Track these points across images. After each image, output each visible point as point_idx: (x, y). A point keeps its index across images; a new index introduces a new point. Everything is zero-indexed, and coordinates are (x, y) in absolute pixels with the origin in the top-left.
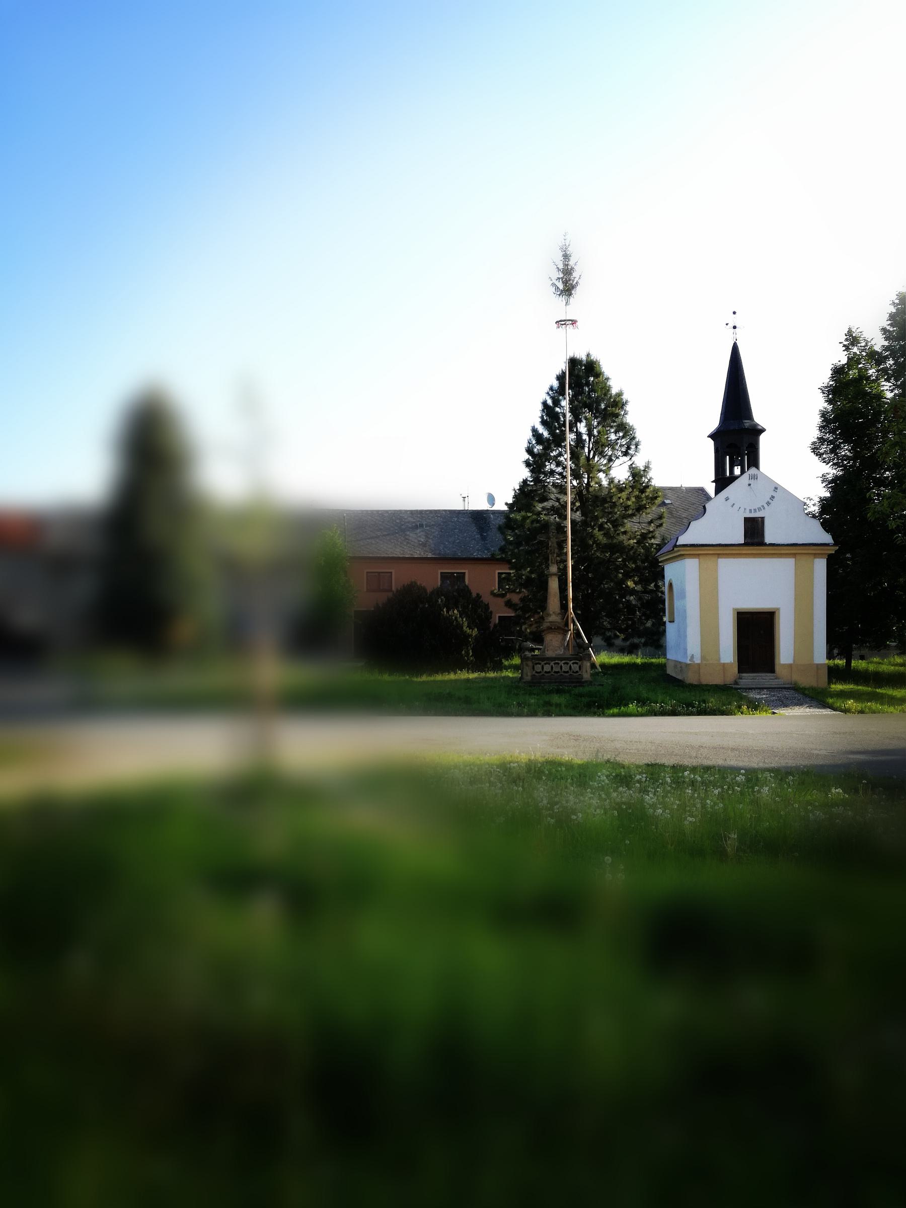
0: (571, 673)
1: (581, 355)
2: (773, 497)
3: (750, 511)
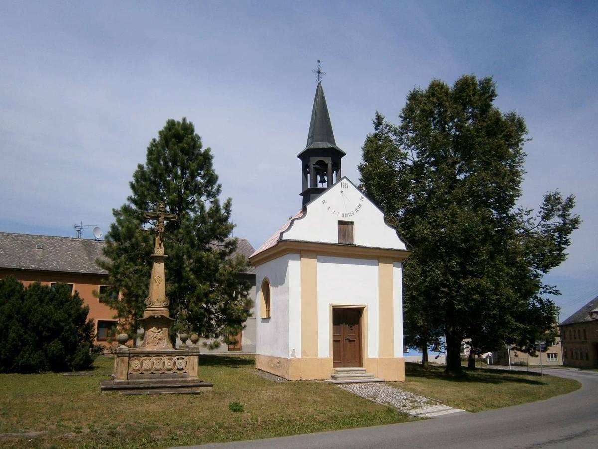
1: (178, 119)
2: (360, 205)
3: (343, 214)
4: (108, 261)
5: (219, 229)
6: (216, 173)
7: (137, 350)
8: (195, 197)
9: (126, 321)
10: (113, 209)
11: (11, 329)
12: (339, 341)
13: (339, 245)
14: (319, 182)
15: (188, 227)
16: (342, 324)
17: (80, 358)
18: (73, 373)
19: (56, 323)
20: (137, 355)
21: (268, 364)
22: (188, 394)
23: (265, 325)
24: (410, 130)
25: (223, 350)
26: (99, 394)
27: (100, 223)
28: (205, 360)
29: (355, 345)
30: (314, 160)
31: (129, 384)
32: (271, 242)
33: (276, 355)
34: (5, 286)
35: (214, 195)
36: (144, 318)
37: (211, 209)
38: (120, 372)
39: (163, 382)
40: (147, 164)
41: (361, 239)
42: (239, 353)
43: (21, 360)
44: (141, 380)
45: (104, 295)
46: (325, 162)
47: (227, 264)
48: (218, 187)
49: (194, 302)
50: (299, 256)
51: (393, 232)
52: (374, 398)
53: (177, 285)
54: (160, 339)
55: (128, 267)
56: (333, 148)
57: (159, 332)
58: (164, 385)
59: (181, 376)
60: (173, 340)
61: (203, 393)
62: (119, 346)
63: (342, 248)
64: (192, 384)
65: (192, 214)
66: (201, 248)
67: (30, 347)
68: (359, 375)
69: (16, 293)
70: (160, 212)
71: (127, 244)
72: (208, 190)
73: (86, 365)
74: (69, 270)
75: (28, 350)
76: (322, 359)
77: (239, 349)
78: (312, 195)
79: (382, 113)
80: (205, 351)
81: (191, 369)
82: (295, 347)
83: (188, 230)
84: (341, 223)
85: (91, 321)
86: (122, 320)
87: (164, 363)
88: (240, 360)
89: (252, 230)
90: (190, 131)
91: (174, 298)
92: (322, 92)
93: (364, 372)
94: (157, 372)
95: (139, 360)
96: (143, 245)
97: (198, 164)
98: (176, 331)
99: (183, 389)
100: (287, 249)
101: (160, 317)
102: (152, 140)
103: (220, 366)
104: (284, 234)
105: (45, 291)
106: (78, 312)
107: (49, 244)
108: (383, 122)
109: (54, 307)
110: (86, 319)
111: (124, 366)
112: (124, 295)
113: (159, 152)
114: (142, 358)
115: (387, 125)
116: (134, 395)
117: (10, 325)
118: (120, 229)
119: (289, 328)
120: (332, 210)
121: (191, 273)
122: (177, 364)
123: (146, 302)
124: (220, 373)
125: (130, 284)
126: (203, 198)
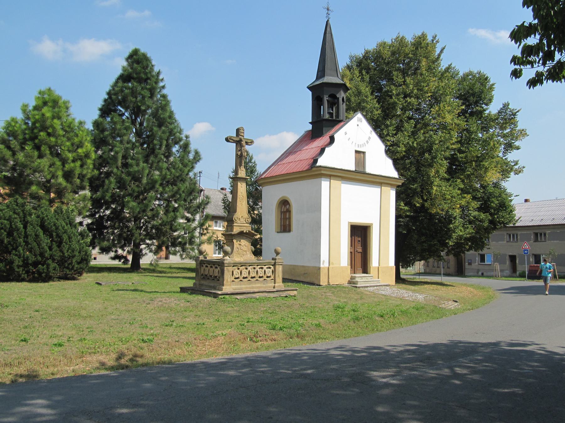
1: (143, 50)
2: (370, 138)
8: (435, 188)
13: (356, 172)
41: (371, 168)
51: (390, 162)
120: (354, 143)
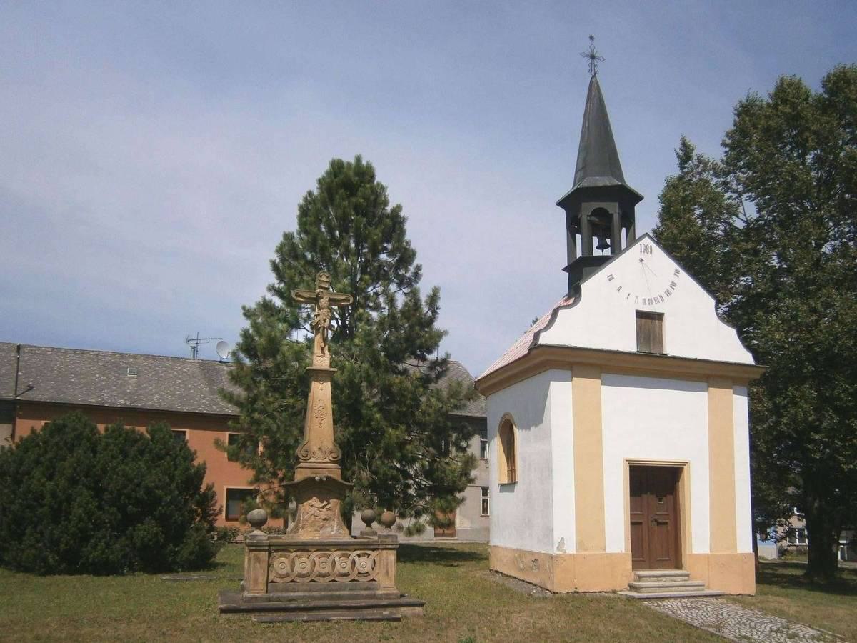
0: (354, 575)
1: (349, 158)
2: (673, 285)
3: (644, 300)
4: (239, 391)
5: (419, 338)
6: (412, 246)
7: (285, 539)
8: (379, 289)
9: (270, 488)
10: (244, 308)
11: (75, 501)
12: (641, 523)
14: (597, 248)
15: (368, 334)
16: (646, 493)
17: (190, 549)
18: (181, 575)
19: (149, 491)
20: (284, 549)
21: (514, 562)
22: (379, 620)
23: (507, 495)
24: (741, 168)
25: (428, 537)
26: (216, 621)
27: (223, 332)
28: (407, 554)
29: (668, 531)
30: (587, 209)
31: (269, 601)
32: (517, 348)
33: (528, 548)
34: (67, 430)
35: (409, 284)
36: (296, 480)
37: (406, 304)
38: (254, 580)
39: (332, 598)
40: (299, 233)
41: (676, 344)
42: (452, 542)
43: (92, 552)
44: (292, 594)
45: (234, 446)
46: (608, 212)
47: (433, 396)
48: (415, 269)
49: (380, 458)
50: (569, 373)
52: (718, 627)
53: (351, 430)
54: (324, 520)
55: (271, 399)
56: (621, 185)
57: (323, 507)
58: (333, 603)
59: (365, 586)
60: (347, 519)
61: (406, 617)
62: (252, 532)
63: (645, 360)
64: (385, 602)
65: (375, 315)
66: (390, 370)
67: (107, 530)
68: (677, 583)
69: (84, 441)
70: (322, 290)
71: (267, 364)
72: (398, 275)
73: (203, 561)
74: (179, 408)
75: (104, 536)
76: (611, 555)
77: (452, 535)
78: (586, 270)
79: (691, 141)
80: (402, 539)
81: (384, 573)
82: (564, 532)
83: (367, 338)
84: (641, 315)
85: (209, 488)
86: (264, 487)
87: (334, 562)
88: (455, 553)
89: (473, 342)
90: (368, 178)
91: (349, 451)
92: (599, 91)
93: (686, 578)
94: (321, 580)
95: (287, 557)
96: (295, 364)
97: (383, 232)
98: (351, 505)
99: (369, 611)
100: (545, 361)
101: (325, 479)
102: (305, 194)
103: (425, 563)
104: (542, 334)
105: (133, 439)
106: (186, 473)
107: (147, 368)
108: (695, 154)
109: (146, 462)
110: (201, 484)
111: (261, 567)
112: (266, 447)
113: (318, 212)
114: (294, 554)
115: (699, 159)
116: (279, 622)
117: (74, 494)
118: (257, 338)
119: (553, 498)
120: (624, 293)
121: (375, 409)
122: (356, 566)
123: (299, 452)
124: (430, 577)
125: (274, 427)
126: (393, 287)
